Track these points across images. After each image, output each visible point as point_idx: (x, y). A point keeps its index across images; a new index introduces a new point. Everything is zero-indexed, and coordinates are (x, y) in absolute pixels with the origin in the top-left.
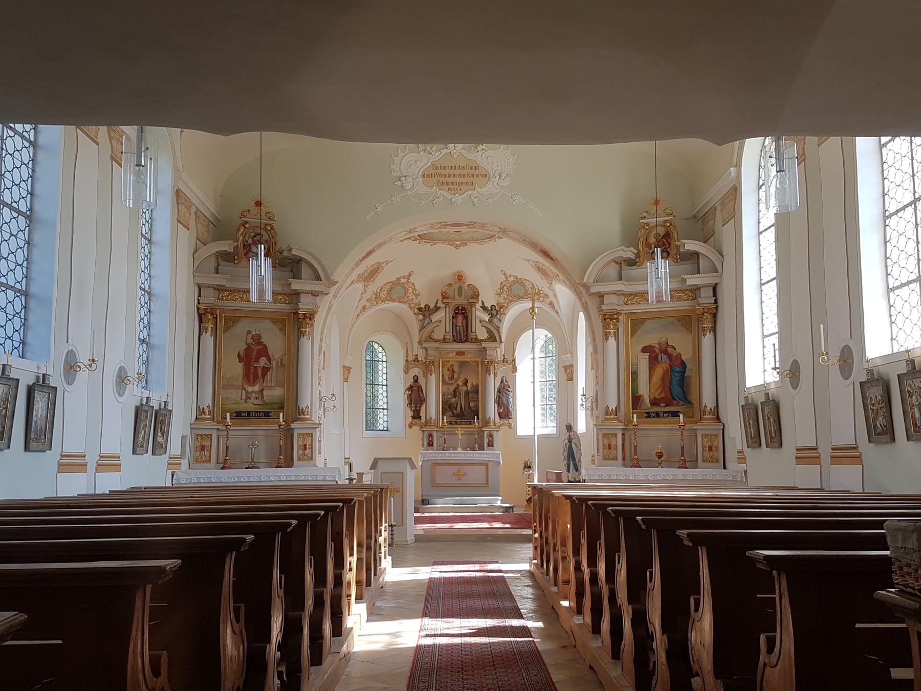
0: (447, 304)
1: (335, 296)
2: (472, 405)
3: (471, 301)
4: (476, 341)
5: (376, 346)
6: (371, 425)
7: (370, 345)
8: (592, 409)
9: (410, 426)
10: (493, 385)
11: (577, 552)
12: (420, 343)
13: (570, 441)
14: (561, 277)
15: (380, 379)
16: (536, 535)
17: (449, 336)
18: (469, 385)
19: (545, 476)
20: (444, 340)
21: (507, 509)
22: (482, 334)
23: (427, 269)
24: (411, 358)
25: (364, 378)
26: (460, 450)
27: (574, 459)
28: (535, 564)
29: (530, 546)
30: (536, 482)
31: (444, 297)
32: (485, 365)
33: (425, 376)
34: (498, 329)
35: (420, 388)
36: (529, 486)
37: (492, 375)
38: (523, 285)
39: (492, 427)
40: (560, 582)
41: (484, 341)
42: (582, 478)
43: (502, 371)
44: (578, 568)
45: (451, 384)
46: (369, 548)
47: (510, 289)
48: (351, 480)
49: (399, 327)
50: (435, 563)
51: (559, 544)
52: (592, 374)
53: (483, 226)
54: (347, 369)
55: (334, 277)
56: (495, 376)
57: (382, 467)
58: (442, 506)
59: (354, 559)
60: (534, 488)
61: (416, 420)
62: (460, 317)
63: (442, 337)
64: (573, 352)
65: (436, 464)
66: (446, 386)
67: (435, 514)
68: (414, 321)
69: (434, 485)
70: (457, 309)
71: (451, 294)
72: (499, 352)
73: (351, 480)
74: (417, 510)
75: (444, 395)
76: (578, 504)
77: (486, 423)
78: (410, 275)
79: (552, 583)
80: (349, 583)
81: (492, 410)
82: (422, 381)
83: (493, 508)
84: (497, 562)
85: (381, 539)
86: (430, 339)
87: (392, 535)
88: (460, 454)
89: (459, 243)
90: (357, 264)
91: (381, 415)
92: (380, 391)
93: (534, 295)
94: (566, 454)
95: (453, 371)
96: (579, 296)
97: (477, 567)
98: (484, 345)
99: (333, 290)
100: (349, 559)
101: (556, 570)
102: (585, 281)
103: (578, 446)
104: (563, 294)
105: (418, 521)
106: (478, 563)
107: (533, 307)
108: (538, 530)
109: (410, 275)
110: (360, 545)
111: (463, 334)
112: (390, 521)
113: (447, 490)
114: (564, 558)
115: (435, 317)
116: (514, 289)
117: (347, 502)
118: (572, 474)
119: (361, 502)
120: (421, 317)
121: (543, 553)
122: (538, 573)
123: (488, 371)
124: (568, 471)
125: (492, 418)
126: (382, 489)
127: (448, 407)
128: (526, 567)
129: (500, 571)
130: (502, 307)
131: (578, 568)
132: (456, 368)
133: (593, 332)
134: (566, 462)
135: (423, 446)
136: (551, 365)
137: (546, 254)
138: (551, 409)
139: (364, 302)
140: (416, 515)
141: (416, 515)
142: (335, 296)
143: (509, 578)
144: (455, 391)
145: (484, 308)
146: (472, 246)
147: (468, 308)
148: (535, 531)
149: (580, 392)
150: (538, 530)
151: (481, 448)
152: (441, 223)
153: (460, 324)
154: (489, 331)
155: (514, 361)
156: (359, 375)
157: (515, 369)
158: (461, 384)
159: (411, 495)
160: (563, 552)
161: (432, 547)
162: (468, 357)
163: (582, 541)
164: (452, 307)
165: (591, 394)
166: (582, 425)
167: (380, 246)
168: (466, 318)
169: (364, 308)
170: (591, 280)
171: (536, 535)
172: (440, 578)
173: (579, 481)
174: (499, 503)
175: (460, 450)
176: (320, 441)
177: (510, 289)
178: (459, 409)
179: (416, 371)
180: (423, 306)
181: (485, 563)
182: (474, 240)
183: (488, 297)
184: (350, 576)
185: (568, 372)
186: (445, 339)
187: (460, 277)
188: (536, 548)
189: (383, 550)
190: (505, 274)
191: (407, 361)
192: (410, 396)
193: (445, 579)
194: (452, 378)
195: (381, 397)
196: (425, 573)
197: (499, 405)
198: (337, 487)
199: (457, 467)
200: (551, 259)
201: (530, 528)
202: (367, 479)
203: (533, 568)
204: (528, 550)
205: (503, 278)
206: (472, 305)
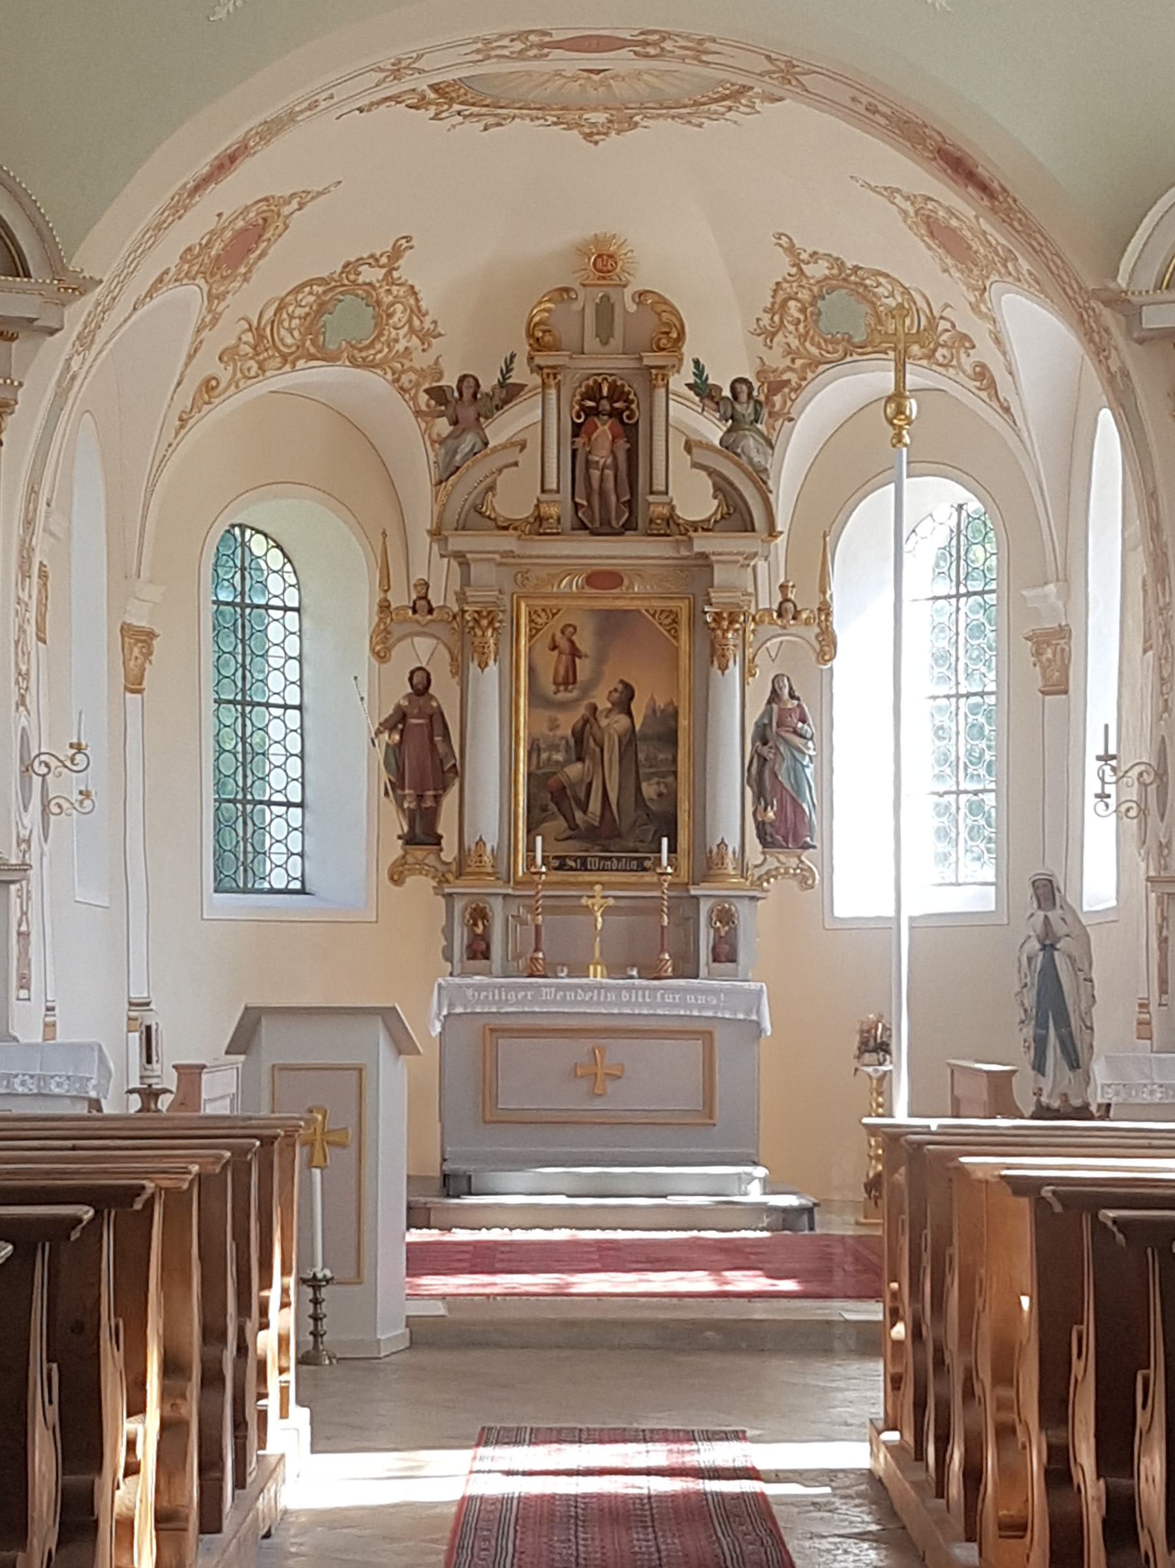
0: (549, 374)
1: (85, 340)
2: (649, 790)
3: (650, 359)
4: (671, 526)
5: (258, 545)
6: (236, 869)
7: (235, 537)
8: (1143, 812)
9: (397, 876)
10: (735, 710)
11: (1055, 1409)
12: (436, 534)
13: (1049, 946)
14: (1025, 266)
15: (275, 681)
16: (899, 1331)
17: (559, 508)
18: (639, 708)
19: (944, 1087)
20: (539, 524)
21: (787, 1218)
22: (693, 499)
23: (472, 227)
24: (400, 598)
25: (209, 675)
26: (597, 976)
27: (1063, 1020)
28: (890, 1447)
29: (875, 1371)
30: (901, 1116)
31: (538, 345)
32: (703, 627)
33: (459, 670)
34: (760, 478)
35: (436, 720)
36: (873, 1130)
37: (735, 670)
38: (865, 295)
39: (732, 882)
40: (990, 1527)
41: (704, 527)
42: (1096, 1100)
43: (774, 651)
44: (1059, 1472)
45: (562, 706)
46: (212, 1379)
47: (812, 311)
48: (150, 1095)
49: (348, 465)
50: (486, 1438)
51: (985, 1374)
52: (1144, 666)
53: (699, 50)
54: (138, 639)
55: (82, 262)
56: (747, 672)
57: (275, 1044)
58: (524, 1200)
59: (146, 1430)
60: (893, 1138)
61: (419, 853)
62: (604, 429)
63: (527, 512)
64: (1069, 574)
65: (497, 1031)
66: (545, 715)
67: (496, 1235)
68: (412, 445)
69: (492, 1116)
70: (593, 393)
71: (566, 330)
72: (759, 575)
73: (150, 1095)
74: (417, 1217)
75: (534, 749)
76: (1065, 1214)
77: (708, 865)
78: (396, 253)
79: (960, 1528)
80: (126, 1526)
81: (730, 812)
82: (444, 692)
83: (734, 1213)
84: (739, 1436)
85: (266, 1342)
86: (478, 516)
87: (316, 1318)
88: (598, 992)
89: (600, 117)
90: (179, 208)
91: (278, 829)
92: (276, 730)
93: (903, 334)
94: (1030, 999)
95: (575, 653)
96: (1097, 343)
97: (658, 1454)
98: (702, 543)
99: (77, 314)
100: (129, 1426)
101: (973, 1475)
102: (1122, 281)
103: (1082, 967)
104: (1032, 333)
105: (422, 1260)
106: (664, 1436)
107: (898, 397)
108: (906, 1309)
109: (396, 253)
110: (172, 1367)
111: (613, 498)
112: (307, 1258)
113: (548, 1134)
114: (1005, 1432)
115: (502, 429)
116: (830, 313)
117: (115, 1200)
118: (1055, 1082)
119: (176, 1201)
120: (443, 426)
121: (925, 1402)
122: (901, 1486)
123: (716, 654)
124: (1039, 1066)
125: (733, 844)
126: (268, 1142)
127: (550, 799)
128: (855, 1455)
129: (750, 1473)
130: (777, 387)
131: (1059, 1472)
132: (585, 641)
133: (1153, 495)
134: (1029, 1031)
135: (448, 956)
136: (976, 630)
137: (959, 167)
138: (975, 809)
139: (208, 365)
140: (416, 1236)
141: (416, 1236)
142: (85, 340)
143: (784, 1500)
144: (579, 736)
145: (703, 390)
146: (658, 132)
147: (635, 388)
148: (895, 1315)
149: (1095, 747)
150: (906, 1309)
151: (687, 968)
152: (522, 36)
153: (601, 456)
154: (723, 488)
155: (825, 609)
156: (188, 659)
157: (826, 645)
158: (603, 704)
159: (395, 1151)
160: (1001, 1406)
161: (482, 1368)
162: (635, 596)
163: (1077, 1366)
164: (572, 384)
165: (1142, 754)
166: (1100, 877)
167: (271, 129)
168: (629, 431)
169: (209, 387)
170: (1148, 279)
171: (899, 1331)
172: (504, 1502)
173: (1083, 1112)
174: (755, 1194)
175: (597, 976)
176: (24, 936)
177: (812, 311)
178: (595, 805)
179: (422, 650)
180: (450, 381)
181: (691, 1437)
182: (667, 106)
183: (723, 347)
184: (133, 1496)
185: (1048, 659)
186: (540, 519)
187: (604, 262)
188: (895, 1382)
189: (274, 1382)
190: (791, 249)
191: (385, 607)
192: (395, 755)
193: (526, 1502)
194: (568, 679)
195: (276, 754)
196: (448, 1476)
197: (759, 795)
198: (92, 1130)
199: (587, 1044)
200: (984, 187)
201: (876, 1296)
202: (219, 1096)
203: (882, 1464)
204: (864, 1388)
205: (783, 266)
206: (655, 377)
